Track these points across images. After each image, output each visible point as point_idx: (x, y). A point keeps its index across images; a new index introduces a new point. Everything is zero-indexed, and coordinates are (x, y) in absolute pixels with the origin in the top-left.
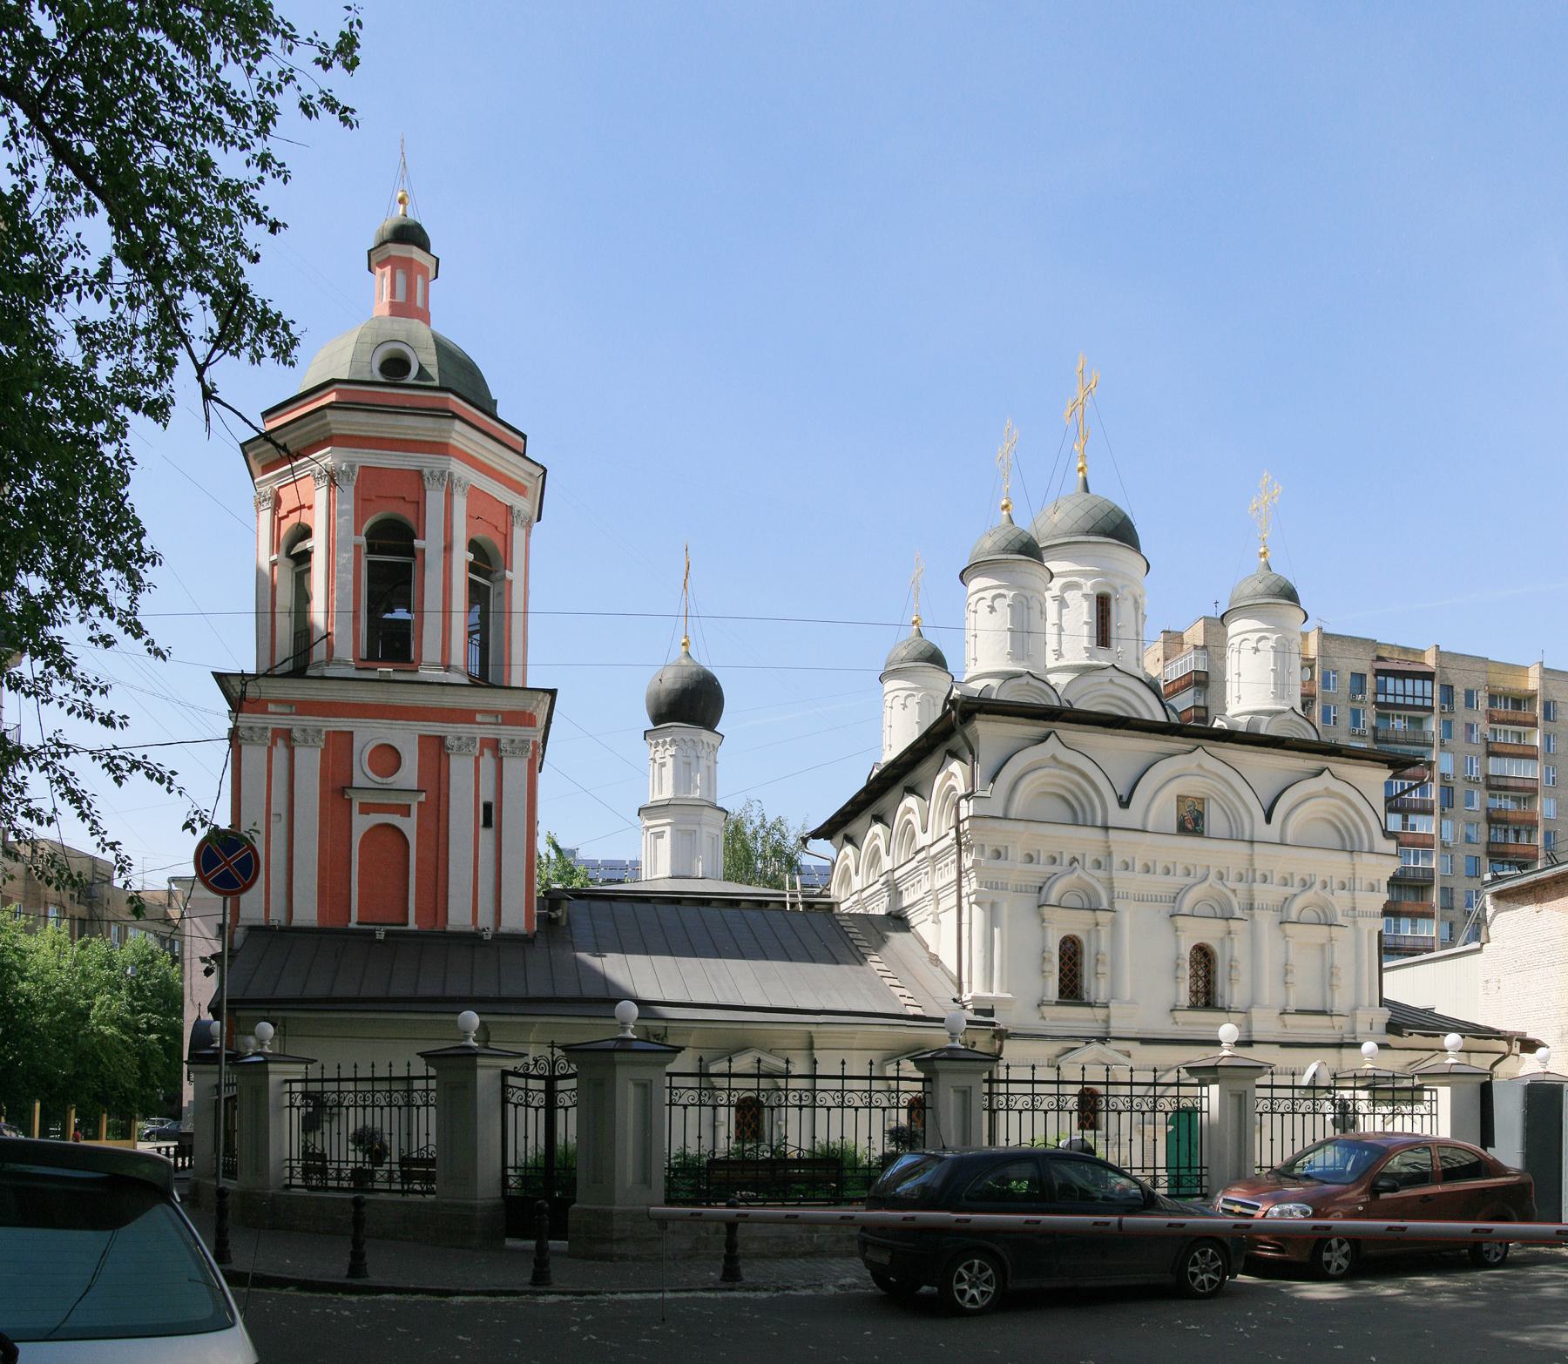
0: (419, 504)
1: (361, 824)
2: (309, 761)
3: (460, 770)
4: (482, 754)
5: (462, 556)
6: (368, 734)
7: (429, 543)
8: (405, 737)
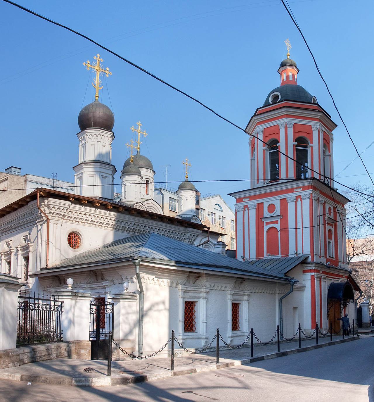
2: (253, 213)
3: (291, 207)
4: (245, 210)
5: (292, 143)
6: (267, 202)
8: (276, 201)
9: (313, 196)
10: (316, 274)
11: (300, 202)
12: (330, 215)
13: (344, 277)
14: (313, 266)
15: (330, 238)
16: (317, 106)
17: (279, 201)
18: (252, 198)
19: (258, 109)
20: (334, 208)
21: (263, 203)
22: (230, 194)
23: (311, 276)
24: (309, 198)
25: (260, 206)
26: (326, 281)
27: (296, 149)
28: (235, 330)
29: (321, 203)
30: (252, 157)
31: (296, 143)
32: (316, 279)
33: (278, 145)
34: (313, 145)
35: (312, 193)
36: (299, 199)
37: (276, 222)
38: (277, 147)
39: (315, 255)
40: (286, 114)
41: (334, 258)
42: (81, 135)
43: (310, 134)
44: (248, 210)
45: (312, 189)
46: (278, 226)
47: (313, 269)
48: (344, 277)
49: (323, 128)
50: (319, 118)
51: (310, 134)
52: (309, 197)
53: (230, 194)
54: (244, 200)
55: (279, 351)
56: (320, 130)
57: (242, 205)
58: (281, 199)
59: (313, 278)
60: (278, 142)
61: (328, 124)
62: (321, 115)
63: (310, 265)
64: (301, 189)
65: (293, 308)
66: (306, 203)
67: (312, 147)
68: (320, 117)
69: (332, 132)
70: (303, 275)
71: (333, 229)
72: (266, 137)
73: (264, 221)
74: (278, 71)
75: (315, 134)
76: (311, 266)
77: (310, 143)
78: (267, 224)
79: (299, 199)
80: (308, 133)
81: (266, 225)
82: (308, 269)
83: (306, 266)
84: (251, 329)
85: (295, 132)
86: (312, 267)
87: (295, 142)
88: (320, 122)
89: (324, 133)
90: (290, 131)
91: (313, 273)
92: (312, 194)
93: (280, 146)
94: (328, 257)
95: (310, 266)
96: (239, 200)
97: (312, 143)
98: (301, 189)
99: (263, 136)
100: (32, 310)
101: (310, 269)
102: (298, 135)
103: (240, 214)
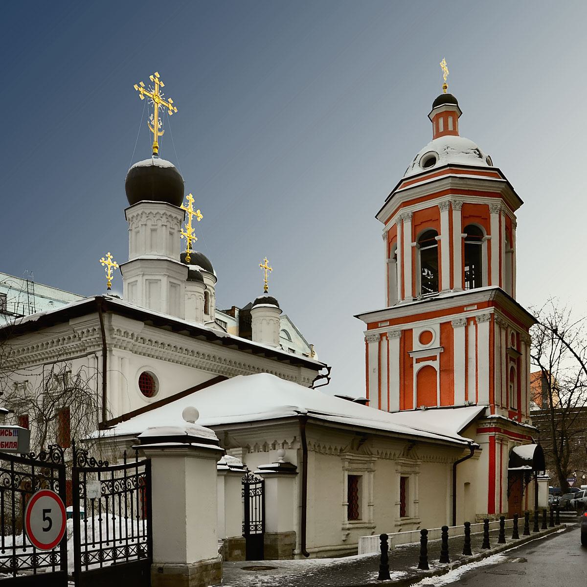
0: (438, 220)
1: (417, 367)
2: (395, 345)
3: (459, 334)
6: (418, 328)
7: (443, 238)
8: (434, 326)
9: (496, 317)
10: (497, 435)
11: (474, 327)
12: (514, 346)
13: (502, 431)
14: (493, 423)
15: (512, 381)
16: (497, 172)
17: (438, 326)
18: (393, 322)
19: (402, 181)
20: (518, 334)
21: (412, 329)
22: (357, 316)
23: (490, 437)
24: (489, 320)
25: (406, 336)
26: (507, 445)
27: (465, 243)
28: (404, 516)
29: (503, 328)
30: (389, 258)
31: (466, 235)
32: (497, 441)
33: (436, 238)
34: (490, 236)
35: (493, 312)
36: (472, 323)
37: (433, 358)
38: (436, 242)
39: (496, 406)
40: (450, 189)
41: (516, 410)
42: (514, 329)
43: (487, 219)
44: (387, 339)
45: (494, 307)
46: (436, 364)
47: (494, 426)
48: (502, 431)
49: (504, 207)
50: (499, 192)
51: (487, 221)
52: (490, 319)
53: (357, 316)
54: (465, 309)
55: (504, 542)
56: (502, 212)
57: (377, 332)
58: (441, 324)
59: (492, 439)
60: (436, 233)
61: (513, 201)
62: (504, 187)
63: (489, 421)
64: (476, 307)
65: (465, 484)
66: (484, 328)
67: (489, 241)
68: (501, 191)
69: (515, 213)
70: (477, 435)
71: (515, 367)
72: (417, 227)
73: (413, 357)
74: (428, 116)
75: (494, 219)
76: (490, 423)
77: (485, 233)
78: (418, 361)
79: (472, 323)
80: (482, 217)
81: (416, 363)
82: (485, 427)
83: (485, 422)
84: (51, 510)
85: (464, 218)
86: (492, 424)
87: (464, 233)
88: (501, 199)
89: (507, 216)
90: (457, 216)
91: (494, 433)
92: (493, 313)
93: (440, 240)
94: (510, 409)
95: (488, 423)
96: (371, 326)
97: (489, 234)
98: (476, 307)
99: (412, 225)
100: (120, 494)
101: (488, 426)
102: (469, 222)
103: (374, 346)
